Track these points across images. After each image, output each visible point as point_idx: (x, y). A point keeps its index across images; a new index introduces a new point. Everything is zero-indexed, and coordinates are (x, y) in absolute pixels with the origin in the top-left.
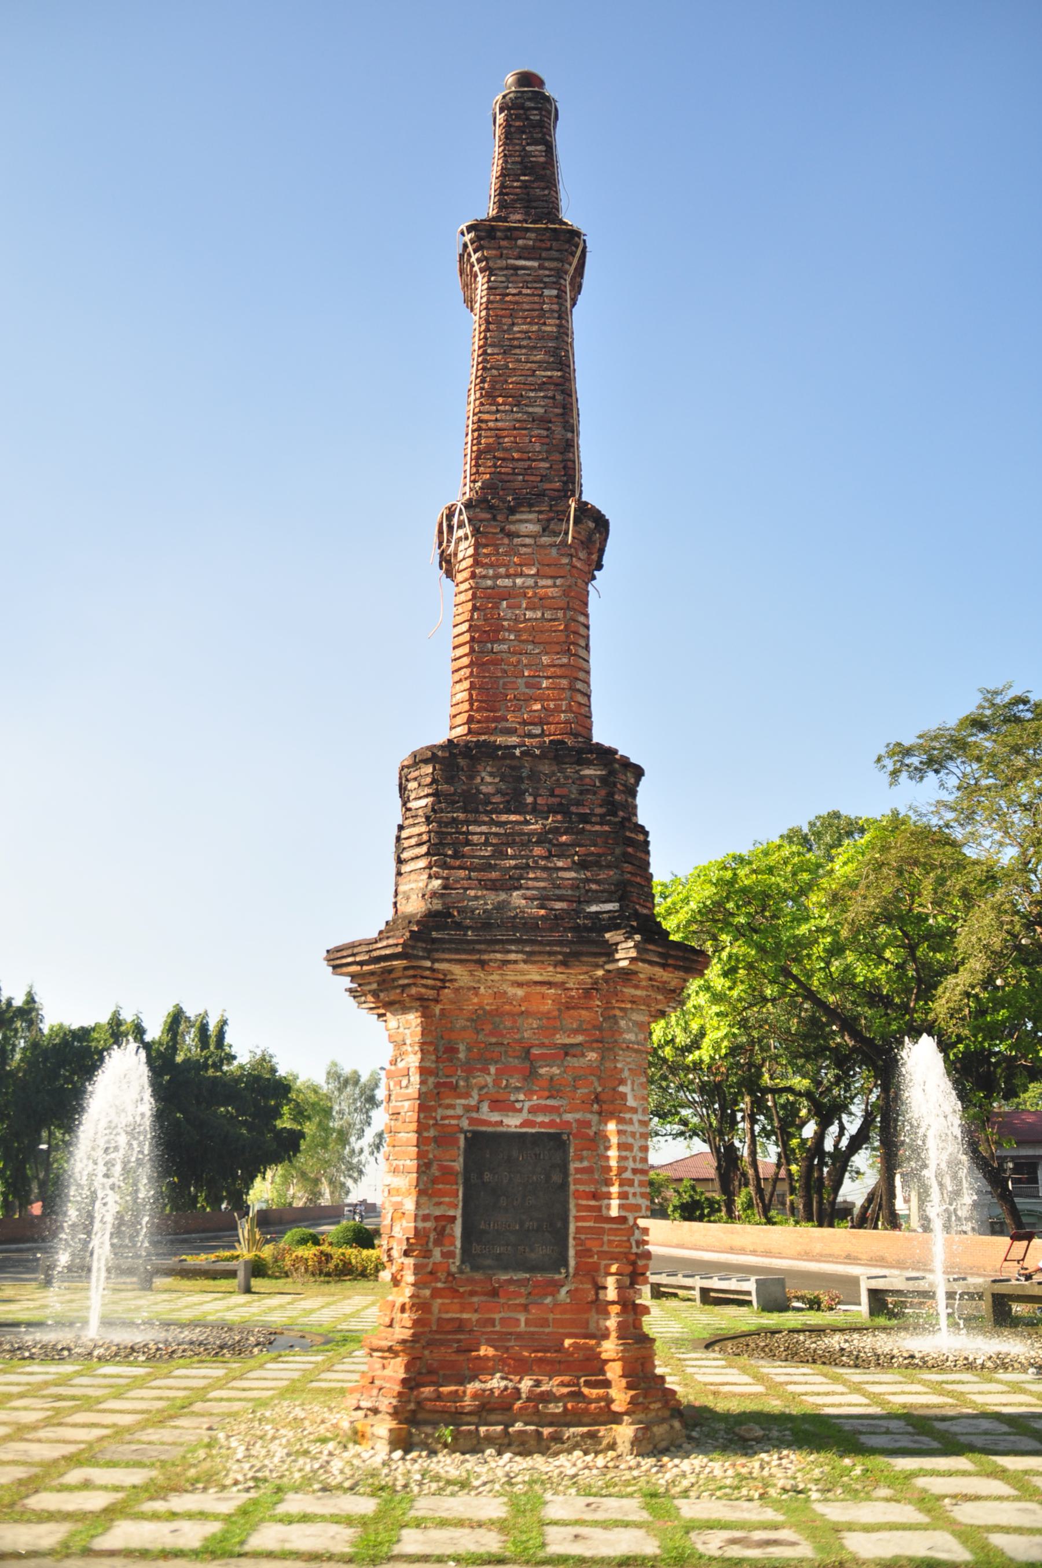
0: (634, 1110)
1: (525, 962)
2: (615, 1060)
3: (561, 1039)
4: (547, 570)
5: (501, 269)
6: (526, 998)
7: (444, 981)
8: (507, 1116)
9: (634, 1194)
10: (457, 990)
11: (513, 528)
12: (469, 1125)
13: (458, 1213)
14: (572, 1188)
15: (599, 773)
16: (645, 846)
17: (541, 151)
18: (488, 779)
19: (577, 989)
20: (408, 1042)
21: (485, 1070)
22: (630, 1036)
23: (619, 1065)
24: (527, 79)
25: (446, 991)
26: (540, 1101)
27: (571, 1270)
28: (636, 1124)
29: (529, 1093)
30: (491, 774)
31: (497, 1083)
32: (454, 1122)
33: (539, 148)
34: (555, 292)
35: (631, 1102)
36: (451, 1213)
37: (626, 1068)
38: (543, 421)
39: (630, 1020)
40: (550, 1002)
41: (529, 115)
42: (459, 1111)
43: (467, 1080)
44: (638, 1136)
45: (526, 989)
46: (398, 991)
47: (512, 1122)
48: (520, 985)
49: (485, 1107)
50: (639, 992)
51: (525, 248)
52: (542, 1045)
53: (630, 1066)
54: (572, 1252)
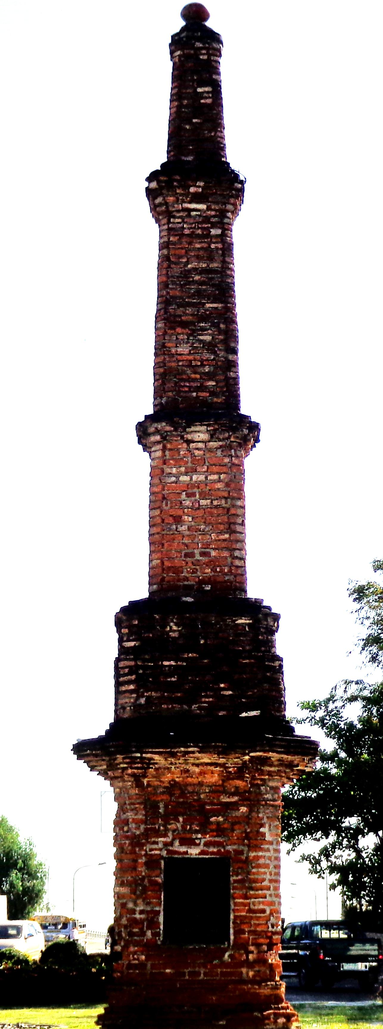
0: (271, 843)
1: (199, 752)
2: (258, 812)
3: (225, 799)
4: (215, 469)
5: (178, 211)
6: (202, 773)
7: (148, 763)
8: (191, 848)
9: (270, 895)
10: (157, 769)
11: (189, 437)
12: (167, 854)
15: (248, 621)
16: (280, 670)
17: (208, 92)
18: (175, 628)
19: (234, 767)
20: (127, 802)
22: (268, 796)
23: (260, 815)
24: (195, 16)
25: (151, 770)
26: (211, 839)
28: (272, 852)
29: (204, 833)
30: (176, 624)
31: (183, 827)
32: (157, 852)
33: (207, 89)
34: (219, 232)
35: (268, 838)
36: (157, 909)
37: (265, 817)
38: (210, 347)
39: (268, 786)
40: (216, 775)
41: (196, 52)
42: (160, 846)
43: (165, 826)
44: (273, 859)
45: (201, 767)
46: (120, 771)
47: (194, 852)
48: (197, 765)
49: (177, 843)
50: (272, 769)
51: (195, 194)
52: (212, 803)
53: (268, 815)
54: (232, 931)
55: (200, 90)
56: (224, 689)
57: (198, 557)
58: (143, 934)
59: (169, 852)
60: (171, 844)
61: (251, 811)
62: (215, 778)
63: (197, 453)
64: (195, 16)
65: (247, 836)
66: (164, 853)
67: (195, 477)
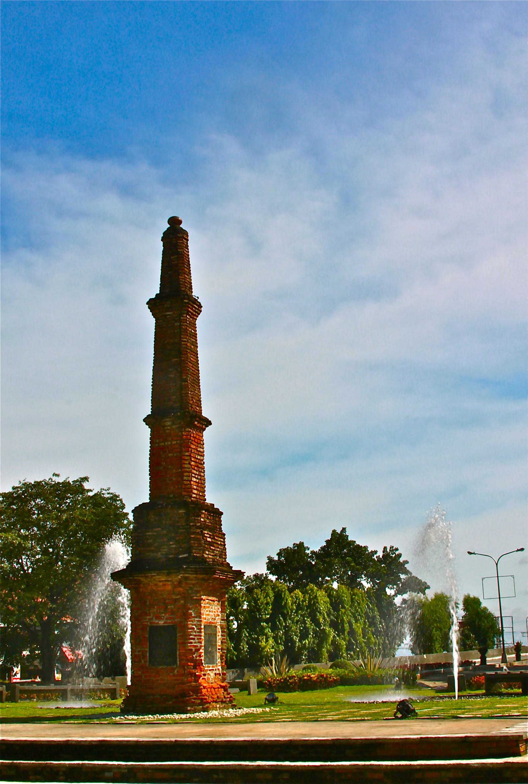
3: (174, 597)
6: (164, 585)
13: (148, 650)
14: (178, 641)
18: (152, 516)
21: (154, 608)
24: (174, 222)
27: (178, 665)
29: (165, 614)
31: (157, 611)
41: (175, 241)
42: (148, 620)
47: (161, 623)
49: (154, 619)
52: (169, 599)
54: (178, 660)
55: (172, 258)
56: (172, 545)
57: (168, 482)
58: (141, 661)
59: (151, 623)
60: (152, 619)
61: (185, 602)
62: (169, 588)
63: (167, 431)
64: (174, 222)
65: (184, 614)
66: (149, 623)
67: (166, 444)
